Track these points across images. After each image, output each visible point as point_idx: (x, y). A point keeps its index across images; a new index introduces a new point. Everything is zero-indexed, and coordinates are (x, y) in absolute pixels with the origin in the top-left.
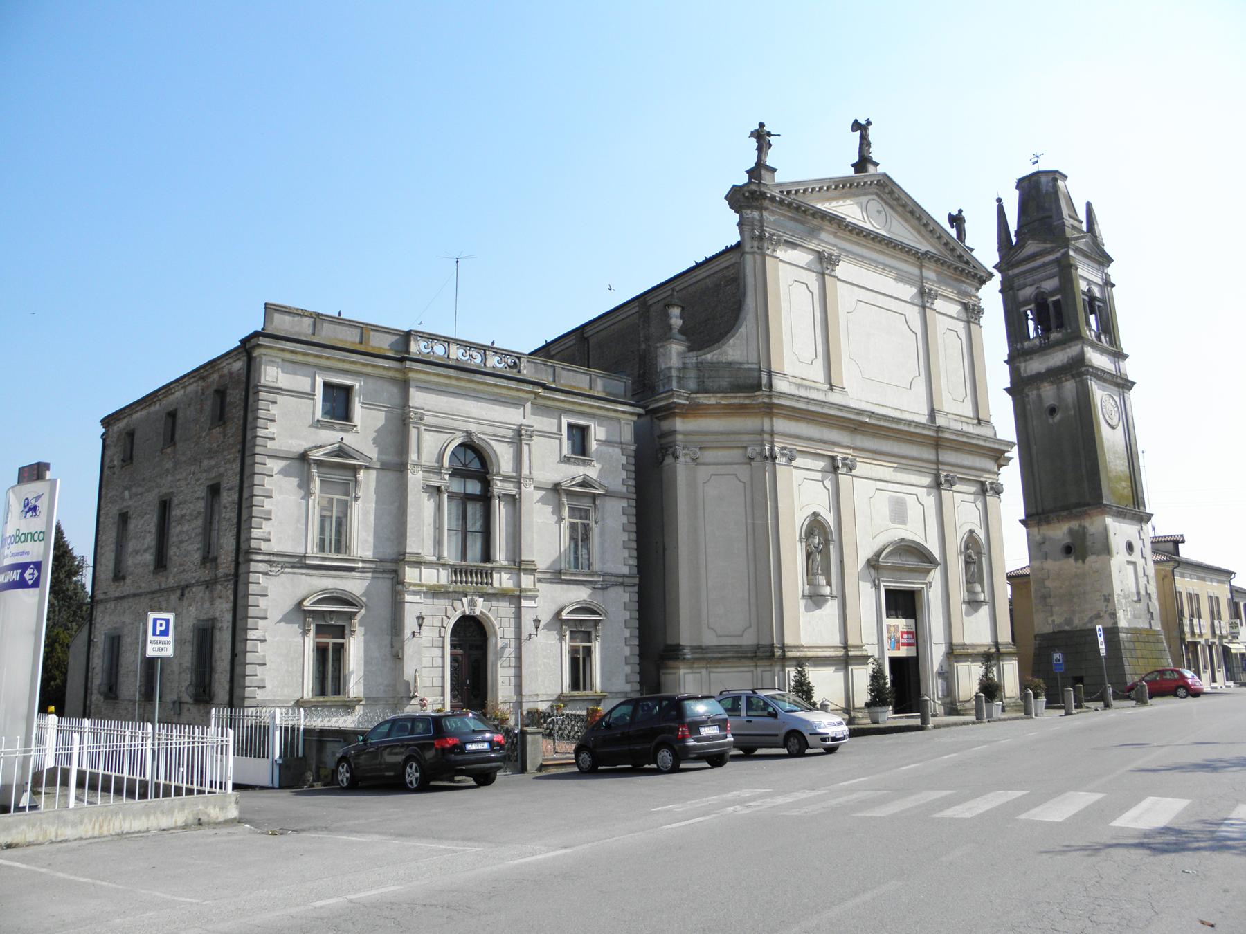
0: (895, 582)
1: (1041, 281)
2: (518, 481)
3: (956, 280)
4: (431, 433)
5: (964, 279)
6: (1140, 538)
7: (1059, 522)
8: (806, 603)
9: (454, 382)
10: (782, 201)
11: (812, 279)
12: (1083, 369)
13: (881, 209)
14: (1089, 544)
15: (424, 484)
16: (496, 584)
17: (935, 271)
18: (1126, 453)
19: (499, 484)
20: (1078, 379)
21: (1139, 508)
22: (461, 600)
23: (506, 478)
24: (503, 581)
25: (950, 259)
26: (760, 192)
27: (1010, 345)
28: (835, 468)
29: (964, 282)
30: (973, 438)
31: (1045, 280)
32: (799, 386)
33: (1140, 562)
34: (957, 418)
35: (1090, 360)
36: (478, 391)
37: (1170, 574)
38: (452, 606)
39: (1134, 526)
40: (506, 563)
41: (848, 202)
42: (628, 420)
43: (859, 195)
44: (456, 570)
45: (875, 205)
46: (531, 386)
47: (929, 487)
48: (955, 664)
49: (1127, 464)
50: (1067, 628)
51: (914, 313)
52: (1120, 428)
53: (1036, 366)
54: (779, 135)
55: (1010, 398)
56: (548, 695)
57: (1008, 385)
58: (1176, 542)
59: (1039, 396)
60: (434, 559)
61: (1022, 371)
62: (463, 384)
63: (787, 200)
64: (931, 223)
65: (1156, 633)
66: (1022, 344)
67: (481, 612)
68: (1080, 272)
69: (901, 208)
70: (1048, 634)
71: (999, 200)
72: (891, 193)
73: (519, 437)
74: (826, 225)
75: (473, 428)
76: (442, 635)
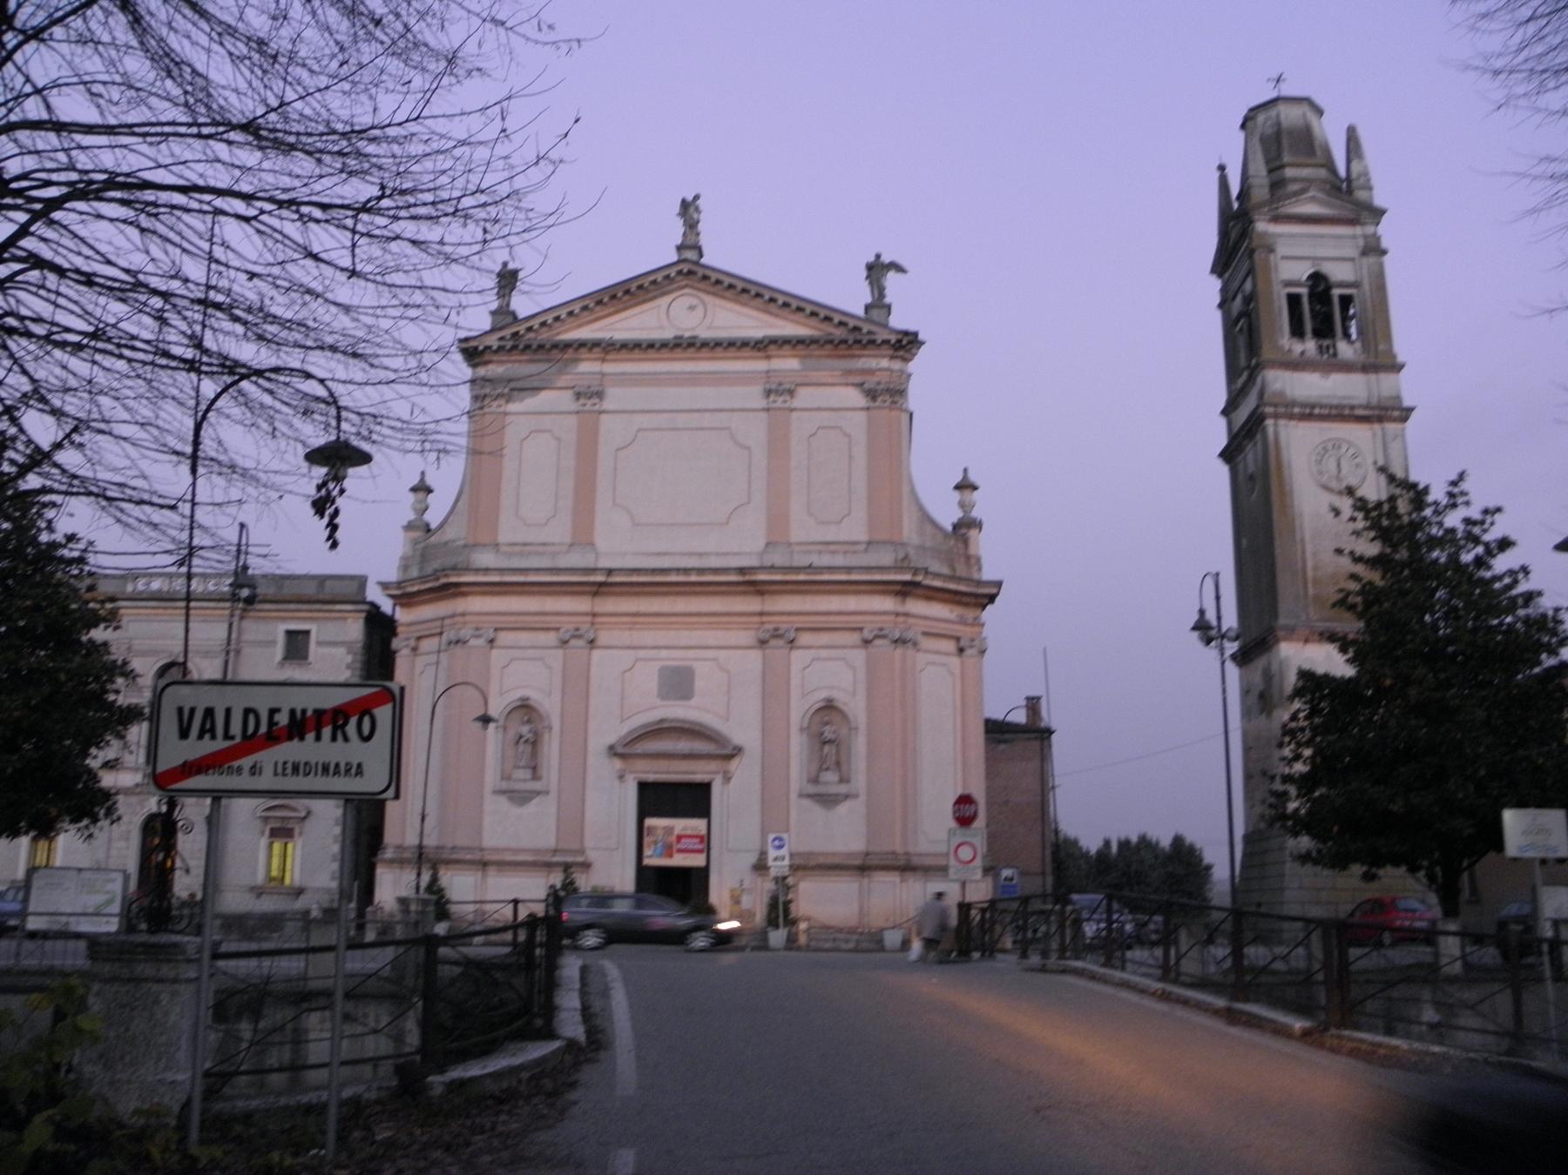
9: (161, 611)
10: (514, 348)
13: (695, 301)
25: (839, 333)
29: (860, 356)
35: (1281, 394)
58: (977, 524)
62: (170, 611)
64: (776, 296)
68: (1282, 249)
74: (583, 353)
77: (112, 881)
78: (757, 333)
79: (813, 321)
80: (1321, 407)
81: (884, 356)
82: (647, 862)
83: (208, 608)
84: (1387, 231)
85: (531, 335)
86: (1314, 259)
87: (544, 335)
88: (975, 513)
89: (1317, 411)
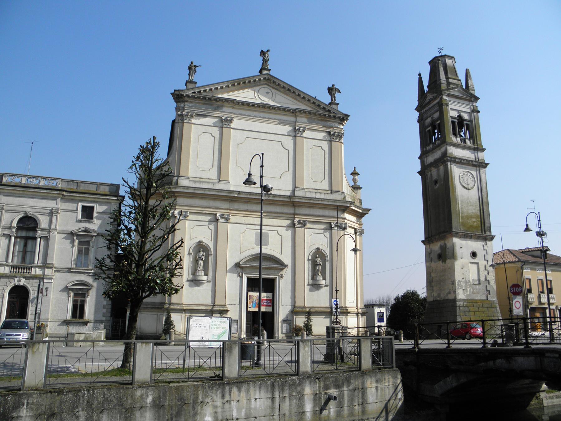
0: (254, 274)
1: (433, 114)
2: (49, 231)
3: (322, 120)
4: (9, 213)
5: (328, 120)
6: (484, 250)
7: (436, 241)
8: (190, 283)
9: (21, 192)
11: (216, 131)
12: (445, 159)
13: (269, 91)
14: (447, 253)
15: (2, 233)
16: (33, 273)
17: (305, 117)
18: (478, 203)
19: (39, 232)
20: (444, 164)
21: (485, 233)
22: (14, 279)
23: (43, 230)
24: (37, 272)
26: (181, 94)
27: (421, 149)
28: (217, 220)
30: (319, 201)
31: (434, 113)
32: (195, 182)
33: (482, 263)
34: (316, 191)
35: (452, 154)
36: (33, 195)
37: (520, 269)
38: (10, 281)
39: (479, 243)
40: (41, 264)
41: (246, 90)
42: (115, 203)
43: (253, 87)
44: (13, 267)
45: (265, 89)
46: (58, 191)
47: (288, 227)
48: (295, 317)
49: (478, 209)
50: (438, 299)
51: (289, 142)
52: (475, 189)
53: (430, 159)
54: (200, 66)
55: (420, 177)
56: (59, 319)
57: (419, 169)
59: (431, 174)
60: (5, 263)
61: (425, 162)
62: (26, 193)
63: (197, 95)
65: (493, 302)
66: (426, 148)
67: (24, 284)
68: (450, 106)
69: (282, 89)
70: (431, 302)
71: (420, 75)
72: (274, 82)
73: (51, 213)
74: (226, 104)
75: (25, 209)
76: (3, 293)
77: (225, 322)
78: (294, 107)
79: (312, 106)
80: (464, 160)
81: (336, 122)
82: (249, 310)
83: (46, 193)
84: (479, 105)
85: (205, 94)
86: (459, 111)
87: (209, 94)
88: (358, 184)
89: (462, 161)
